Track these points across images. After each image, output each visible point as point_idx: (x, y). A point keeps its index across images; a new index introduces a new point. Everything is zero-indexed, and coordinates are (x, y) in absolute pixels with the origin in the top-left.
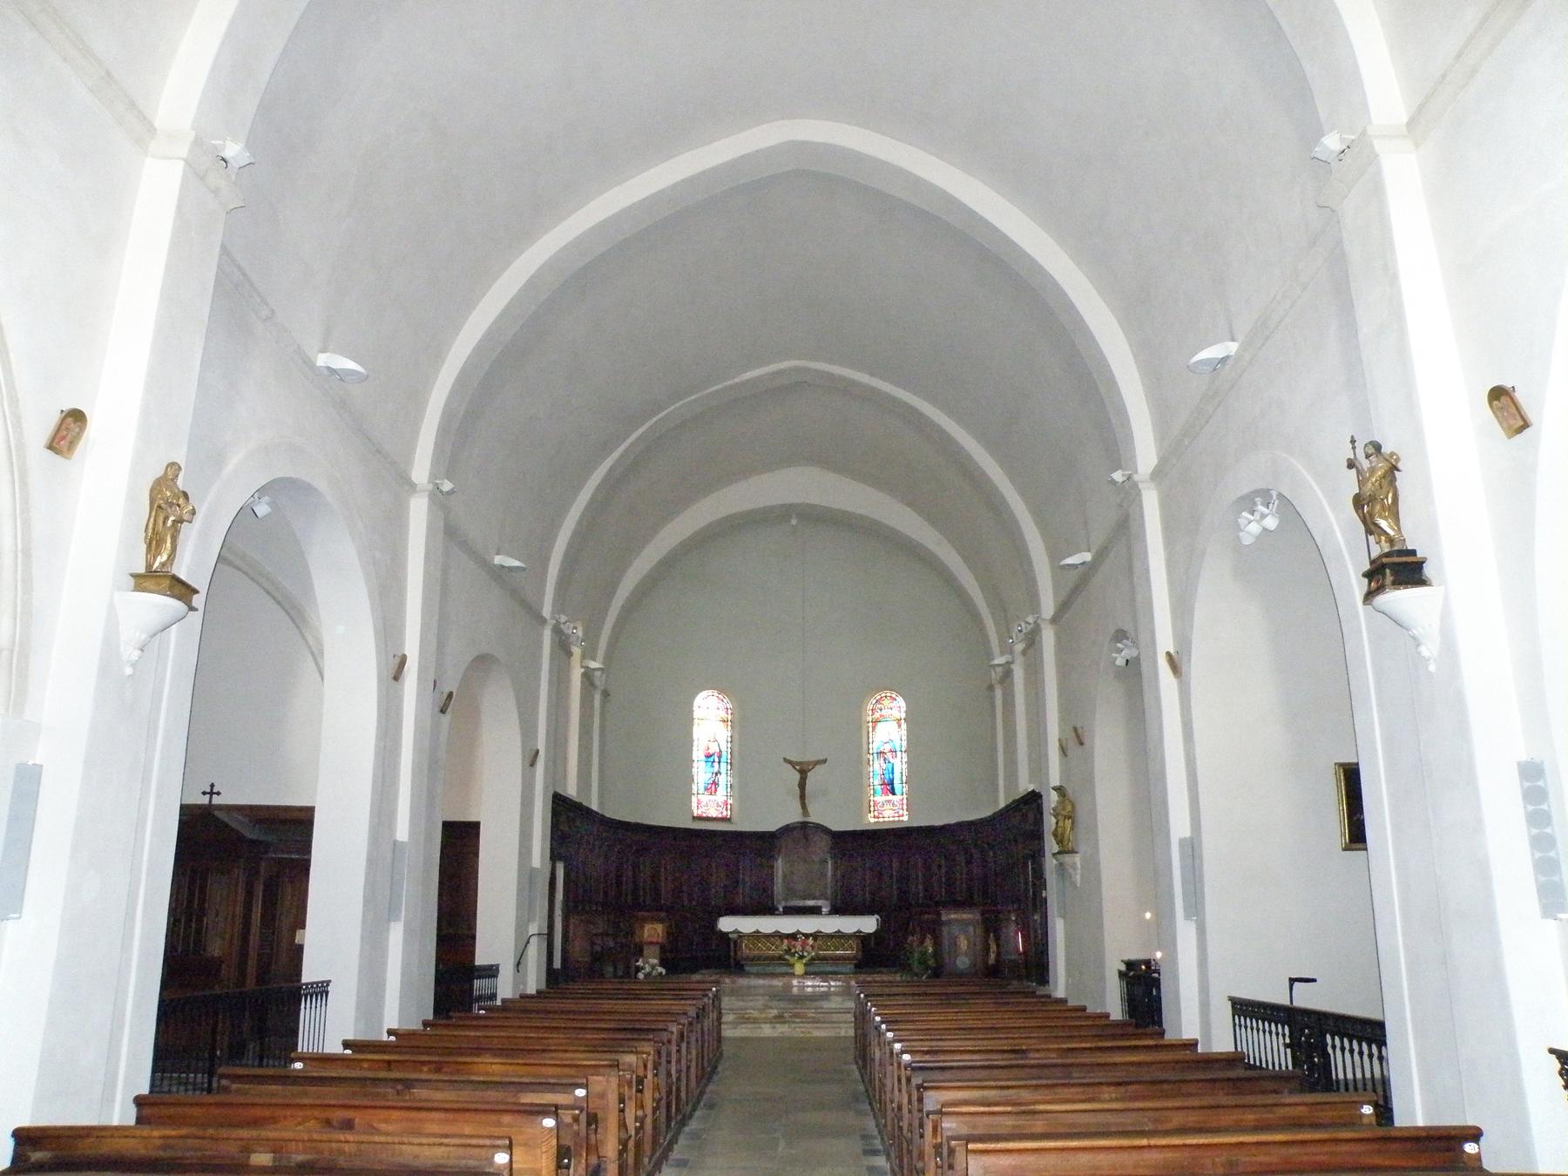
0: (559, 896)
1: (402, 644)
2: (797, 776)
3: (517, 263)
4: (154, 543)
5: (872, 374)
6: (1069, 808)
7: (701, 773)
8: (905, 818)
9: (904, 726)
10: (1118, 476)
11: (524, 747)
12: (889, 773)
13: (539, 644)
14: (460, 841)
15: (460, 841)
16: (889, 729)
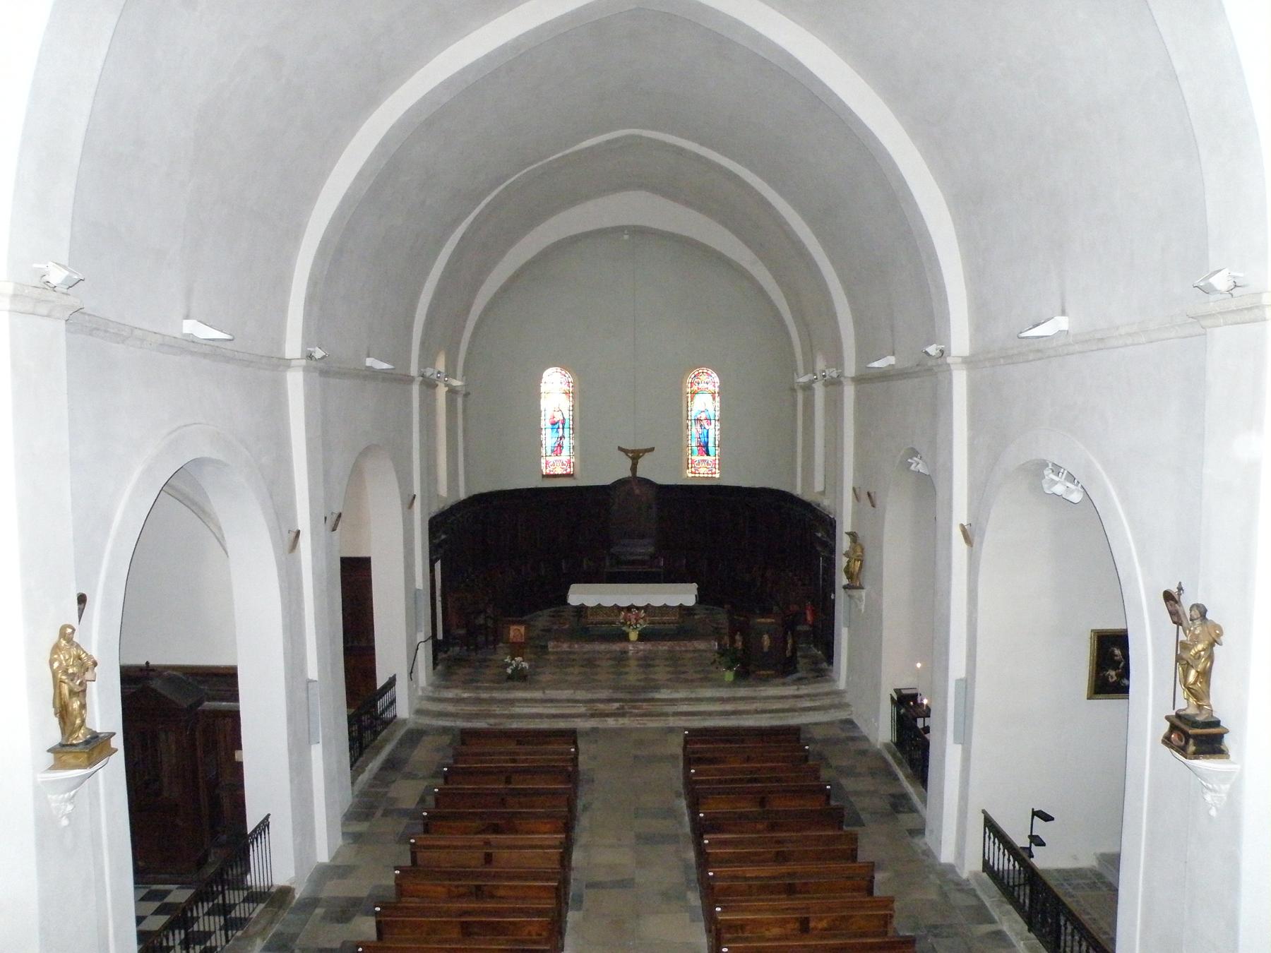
0: (438, 593)
1: (294, 519)
2: (629, 463)
3: (365, 128)
4: (63, 713)
5: (702, 144)
6: (859, 550)
7: (549, 439)
8: (717, 476)
9: (718, 399)
10: (932, 350)
11: (402, 494)
12: (703, 437)
13: (409, 403)
14: (355, 577)
15: (355, 577)
16: (704, 400)
